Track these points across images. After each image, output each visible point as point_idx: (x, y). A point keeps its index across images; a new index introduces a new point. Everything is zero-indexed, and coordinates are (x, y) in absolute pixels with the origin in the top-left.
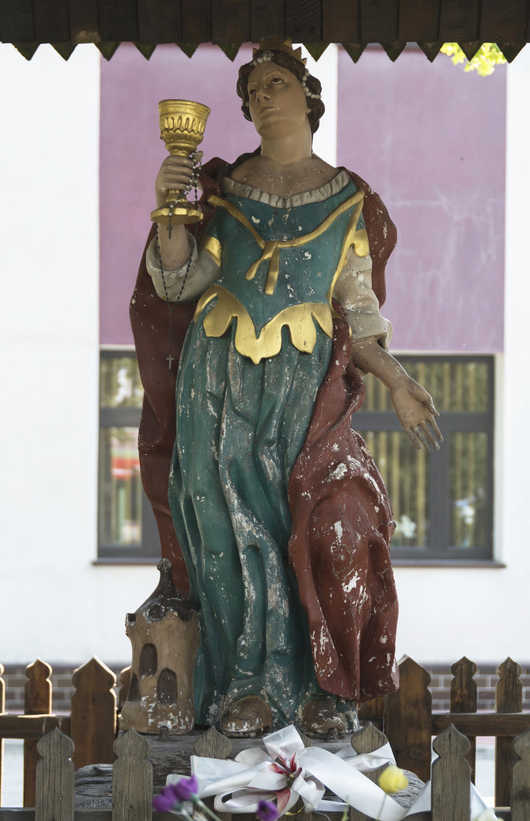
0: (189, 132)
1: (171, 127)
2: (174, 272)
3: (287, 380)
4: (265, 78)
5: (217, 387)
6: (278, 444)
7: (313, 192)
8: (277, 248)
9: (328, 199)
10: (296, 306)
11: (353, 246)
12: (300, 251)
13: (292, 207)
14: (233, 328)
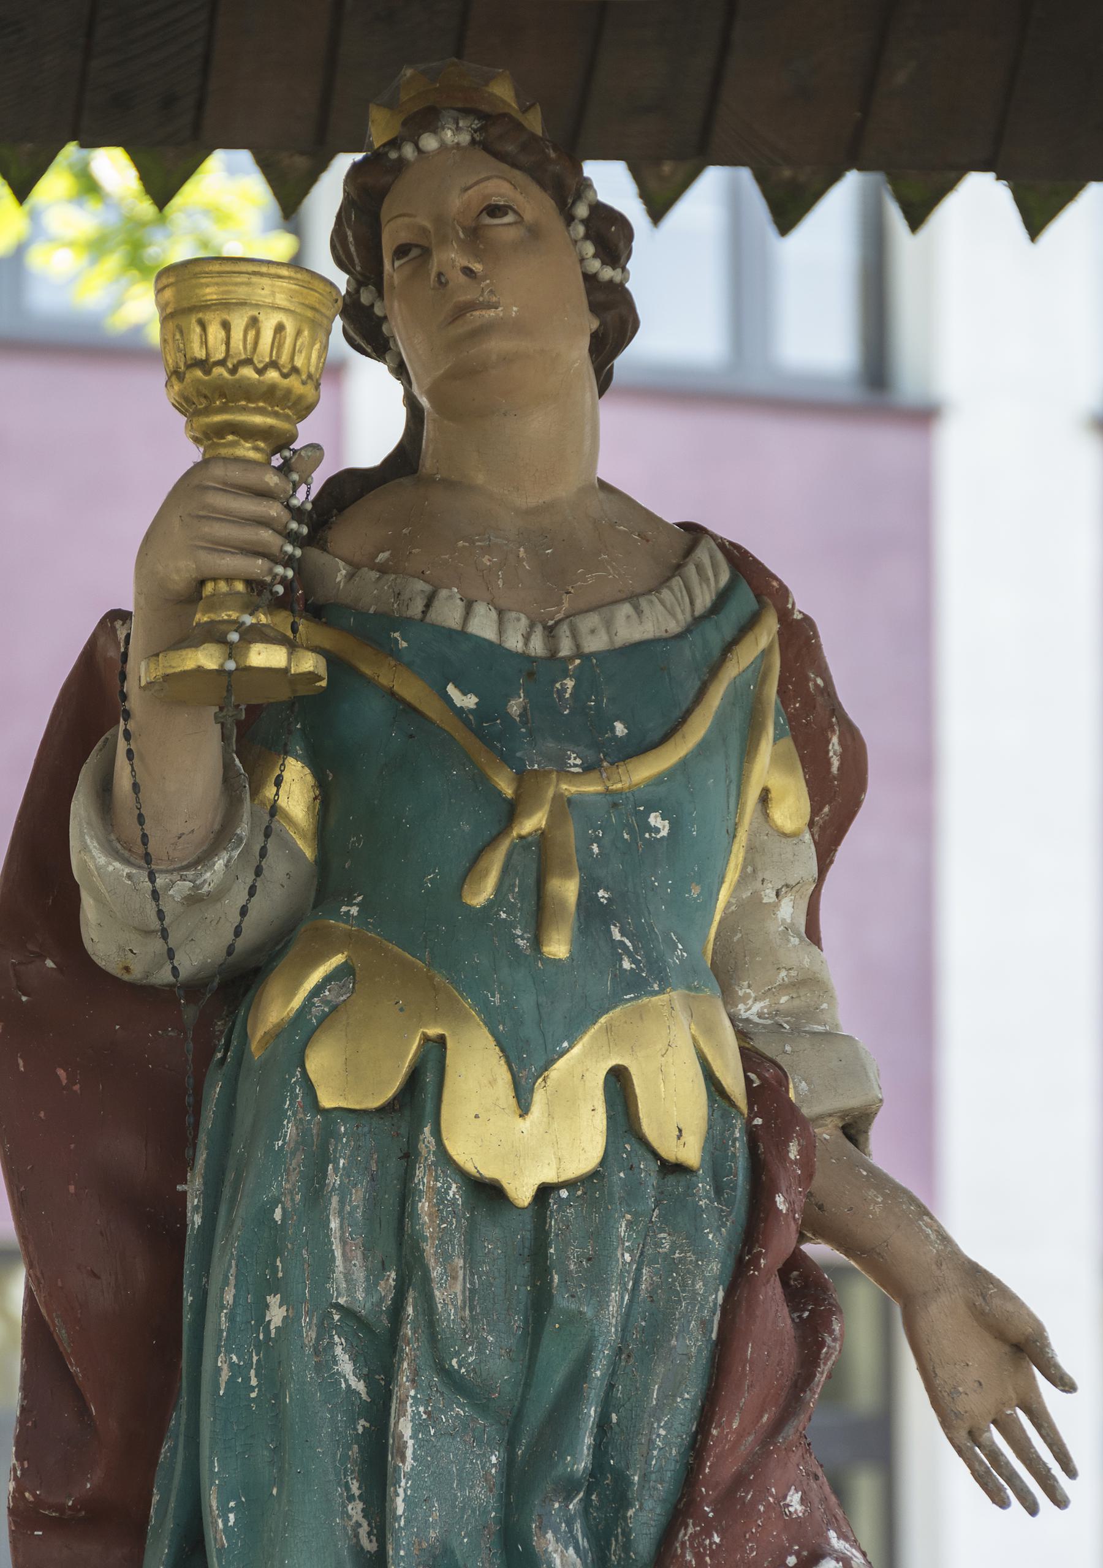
0: (285, 376)
1: (219, 355)
2: (183, 879)
3: (624, 1263)
4: (456, 202)
5: (368, 1291)
6: (588, 1494)
7: (643, 602)
8: (558, 797)
9: (688, 630)
10: (645, 1000)
11: (765, 797)
12: (632, 808)
13: (579, 654)
14: (429, 1078)
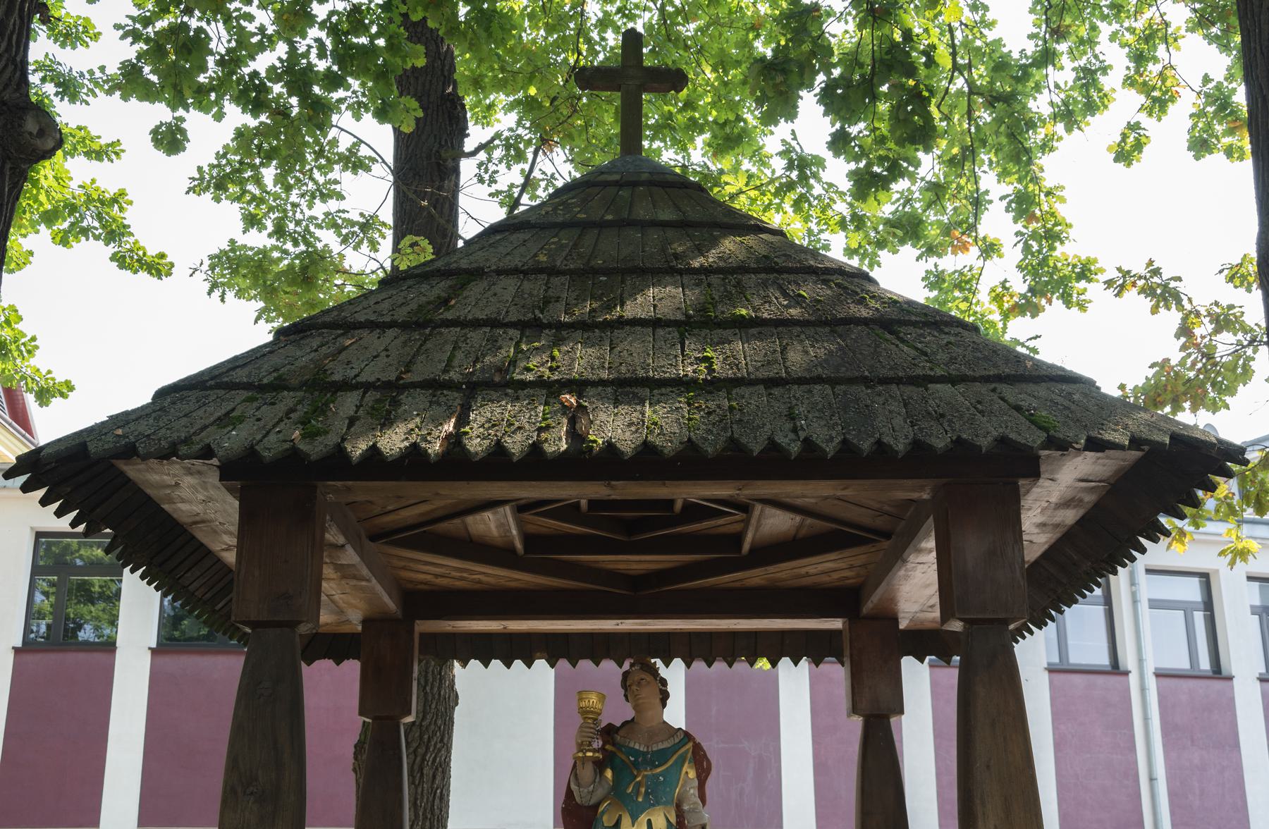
12: (656, 776)
